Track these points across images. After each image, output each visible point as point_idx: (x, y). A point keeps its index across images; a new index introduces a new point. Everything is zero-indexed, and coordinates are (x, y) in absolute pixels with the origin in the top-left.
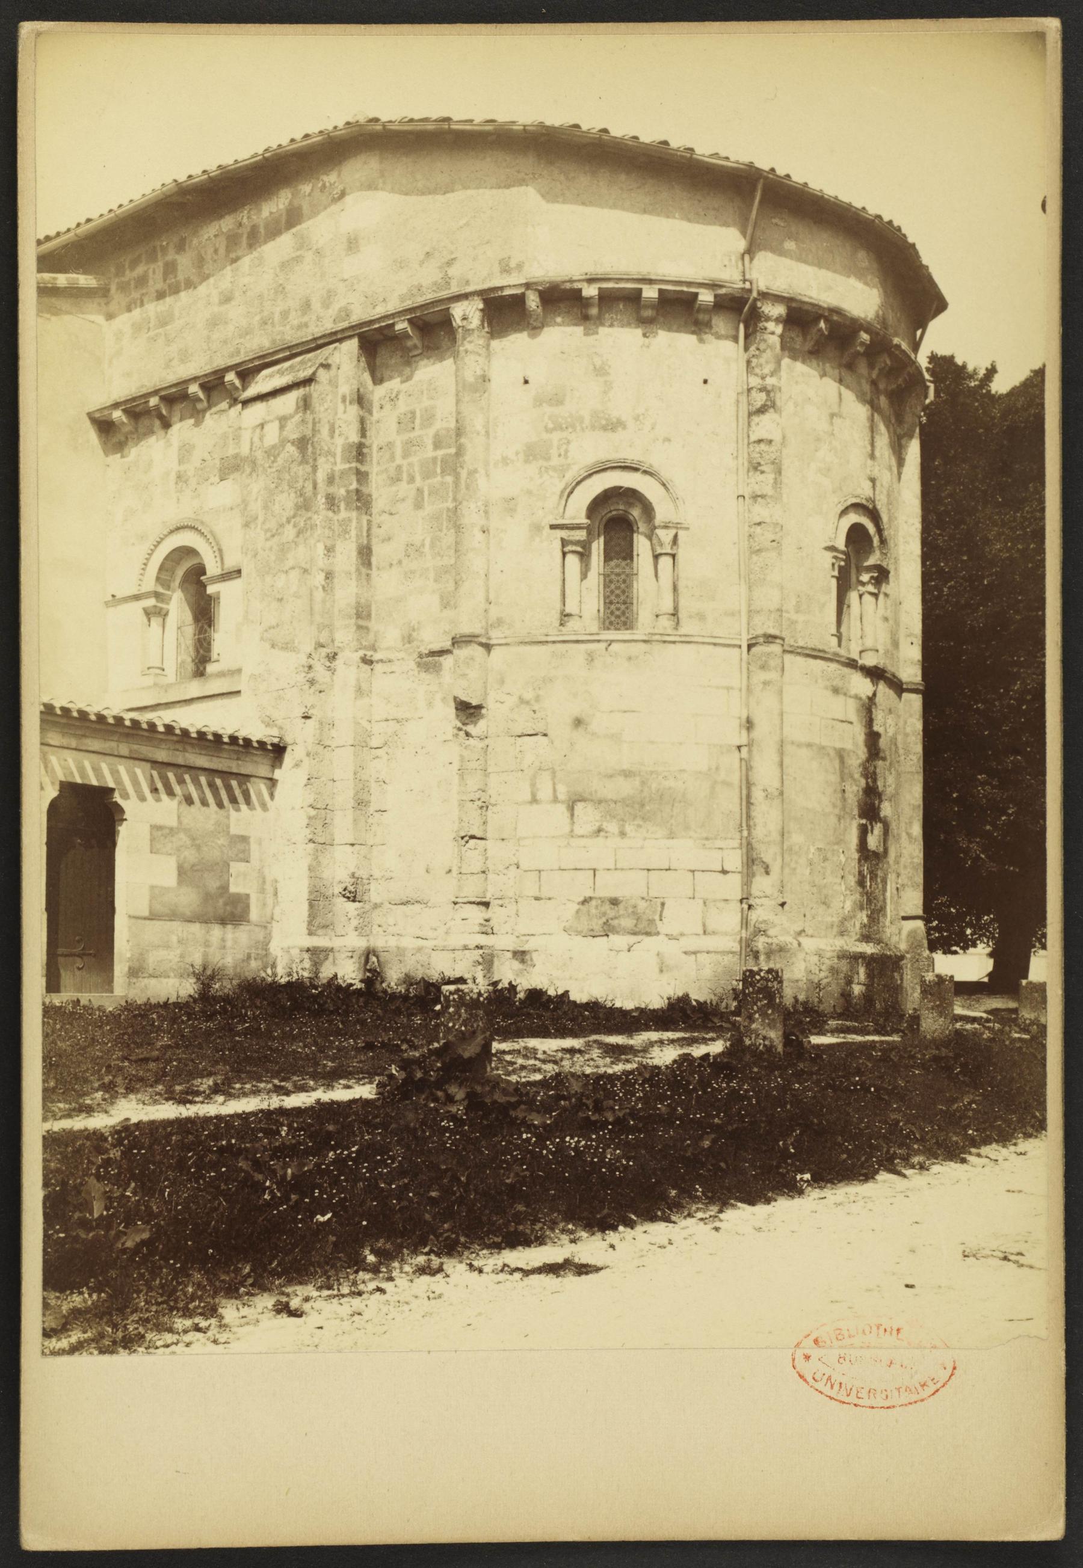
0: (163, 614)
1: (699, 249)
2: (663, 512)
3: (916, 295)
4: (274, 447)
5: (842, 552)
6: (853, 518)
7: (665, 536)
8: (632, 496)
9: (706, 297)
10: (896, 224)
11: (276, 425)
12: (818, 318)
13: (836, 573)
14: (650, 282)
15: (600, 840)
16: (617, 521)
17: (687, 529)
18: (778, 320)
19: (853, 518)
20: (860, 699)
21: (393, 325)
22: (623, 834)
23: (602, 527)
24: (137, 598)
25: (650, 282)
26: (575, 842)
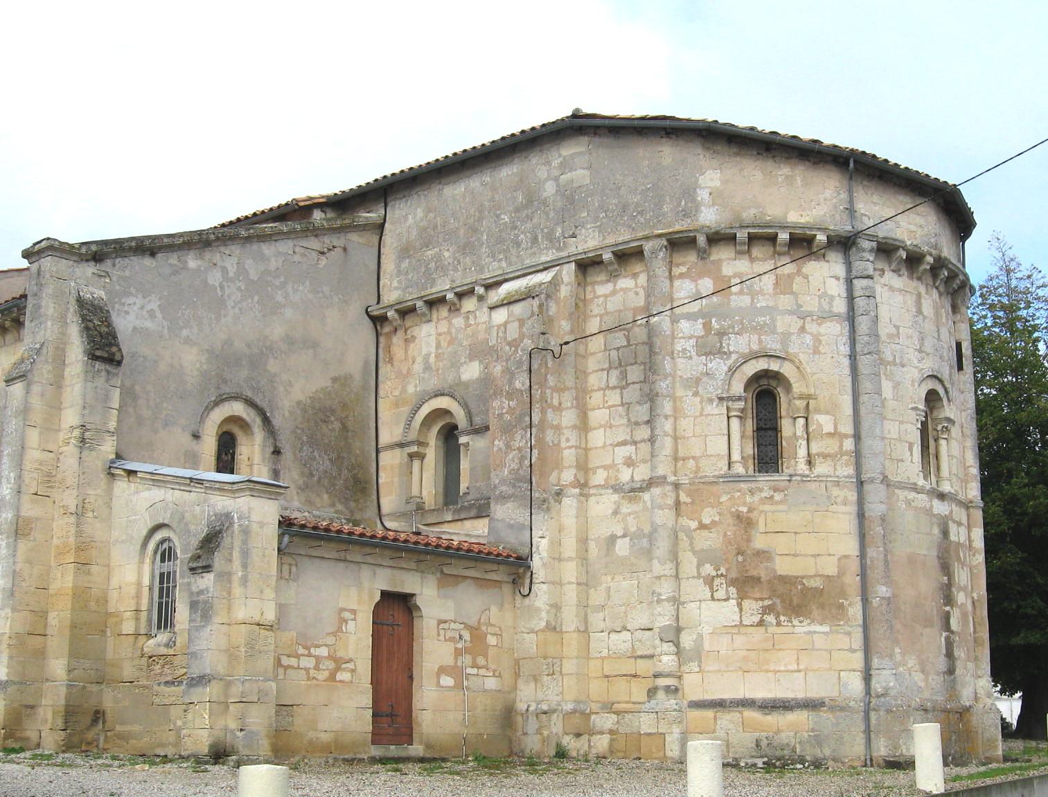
0: (421, 457)
1: (813, 201)
2: (797, 388)
3: (954, 212)
4: (515, 340)
5: (923, 411)
6: (931, 384)
7: (801, 404)
8: (777, 376)
9: (821, 238)
10: (972, 210)
11: (516, 324)
12: (897, 248)
13: (919, 426)
14: (784, 227)
15: (762, 629)
16: (765, 395)
17: (816, 399)
18: (871, 251)
19: (931, 384)
20: (590, 410)
21: (601, 255)
22: (779, 624)
23: (754, 396)
24: (401, 445)
25: (784, 227)
26: (743, 630)
